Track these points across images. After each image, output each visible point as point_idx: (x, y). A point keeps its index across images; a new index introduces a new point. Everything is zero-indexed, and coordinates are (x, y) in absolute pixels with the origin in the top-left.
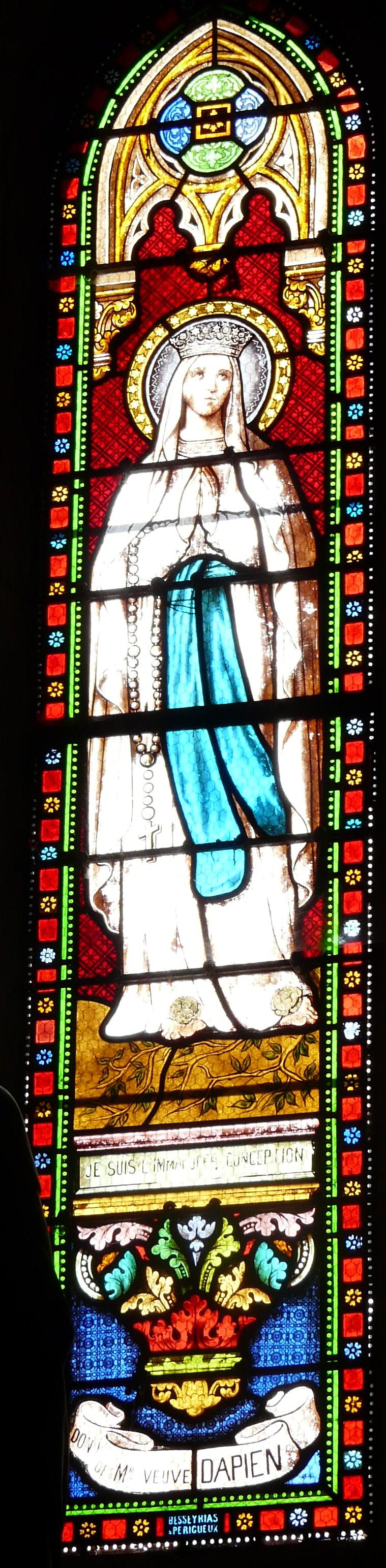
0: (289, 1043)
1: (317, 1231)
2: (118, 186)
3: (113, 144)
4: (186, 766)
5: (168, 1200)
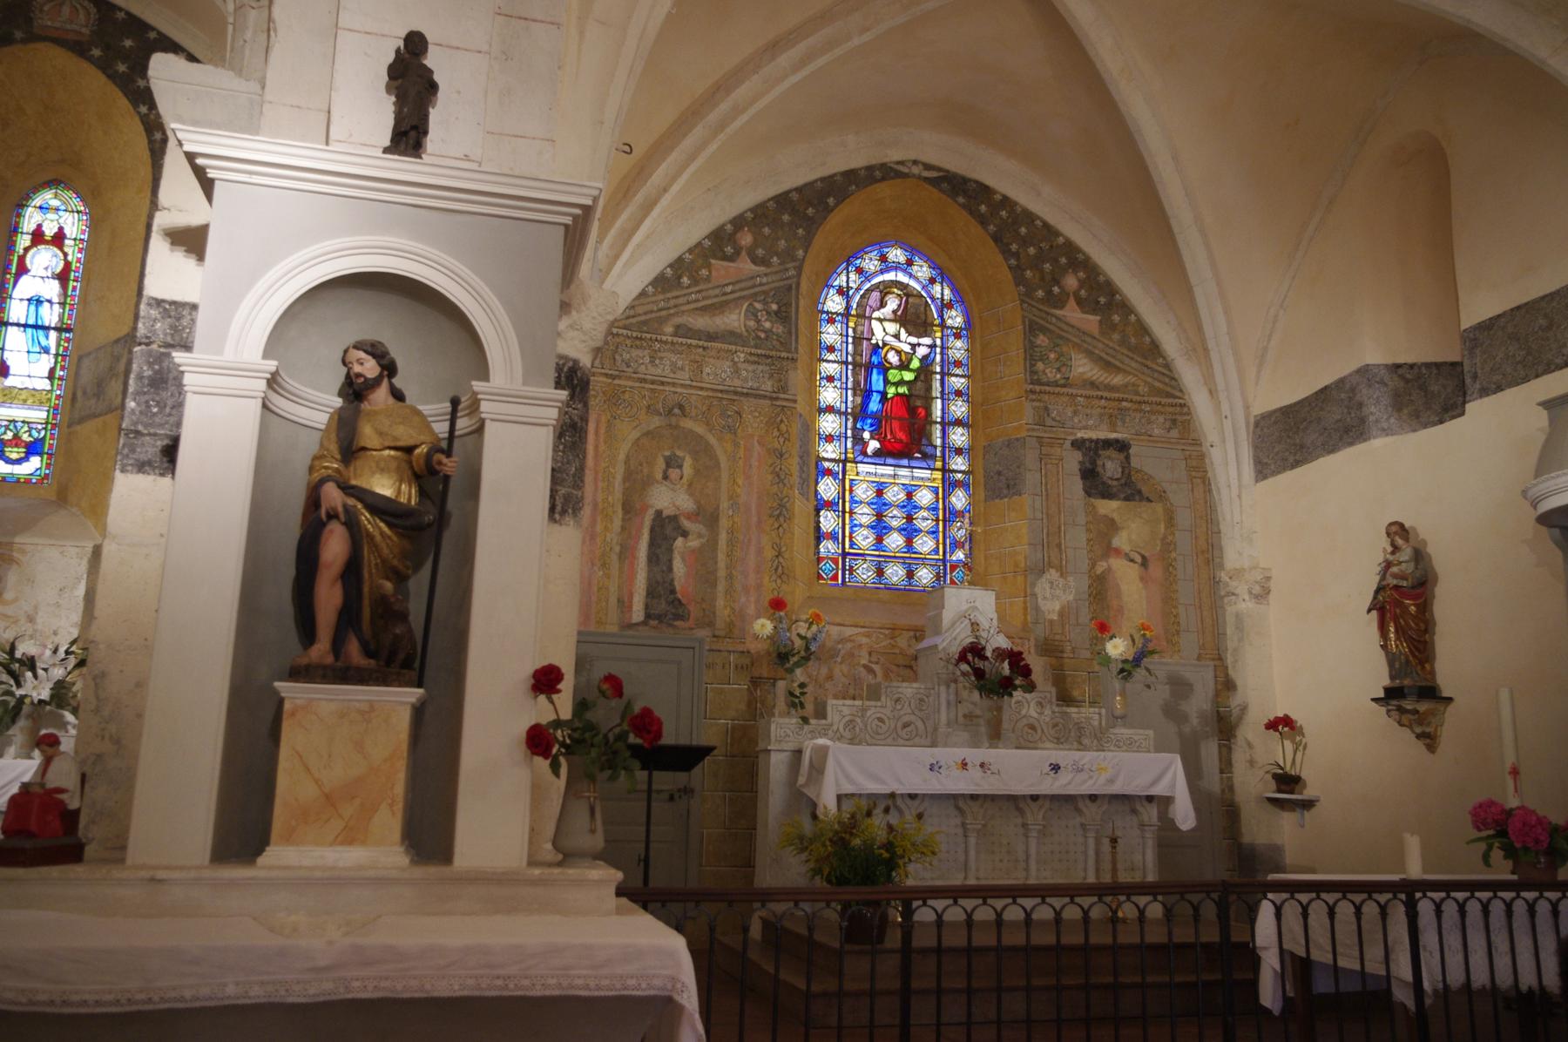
1: (45, 429)
2: (30, 217)
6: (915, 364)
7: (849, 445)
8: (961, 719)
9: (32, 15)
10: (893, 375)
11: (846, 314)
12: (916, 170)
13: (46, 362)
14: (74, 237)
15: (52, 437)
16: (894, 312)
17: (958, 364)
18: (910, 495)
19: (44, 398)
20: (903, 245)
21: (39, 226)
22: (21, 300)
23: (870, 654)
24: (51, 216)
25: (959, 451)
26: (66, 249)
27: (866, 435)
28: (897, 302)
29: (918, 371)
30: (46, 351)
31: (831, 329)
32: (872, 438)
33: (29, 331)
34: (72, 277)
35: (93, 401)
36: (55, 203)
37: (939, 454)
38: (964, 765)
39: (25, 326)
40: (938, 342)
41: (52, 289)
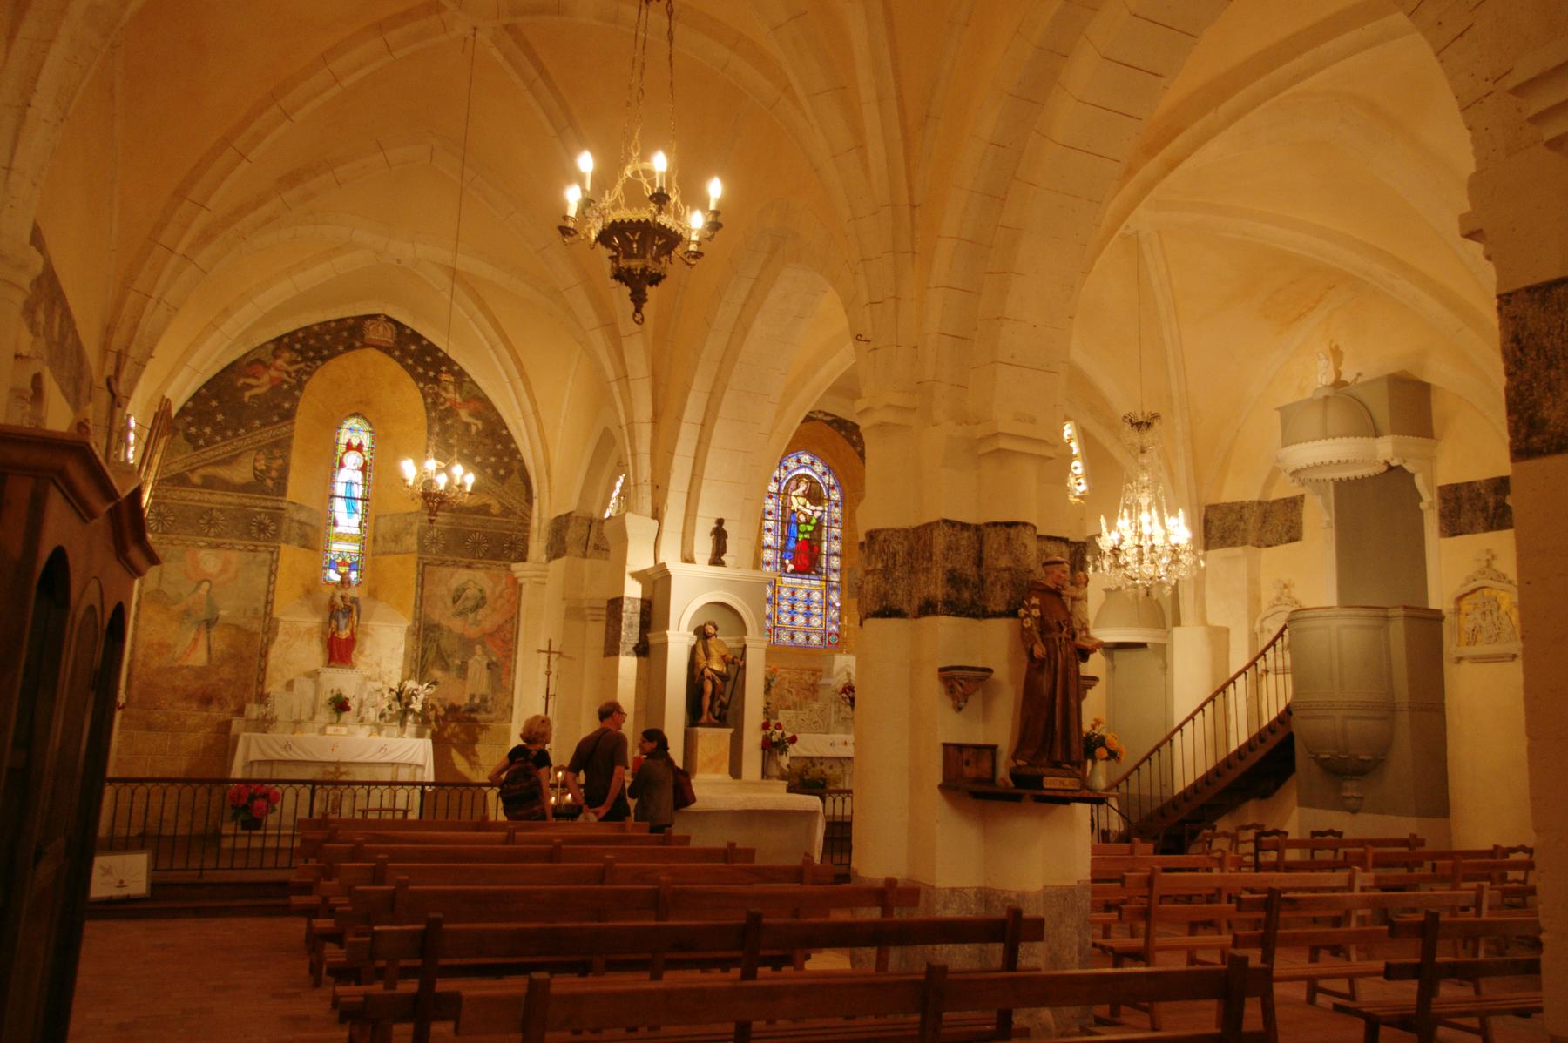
6: (814, 521)
7: (778, 567)
8: (840, 720)
10: (802, 528)
11: (778, 493)
12: (820, 416)
13: (357, 518)
15: (362, 561)
16: (804, 492)
17: (836, 521)
18: (809, 595)
20: (808, 452)
23: (790, 683)
24: (355, 434)
25: (835, 570)
26: (364, 453)
27: (787, 561)
28: (805, 486)
29: (815, 525)
30: (356, 512)
31: (770, 501)
32: (791, 563)
33: (347, 500)
36: (357, 426)
37: (824, 571)
38: (846, 743)
40: (826, 509)
41: (358, 476)
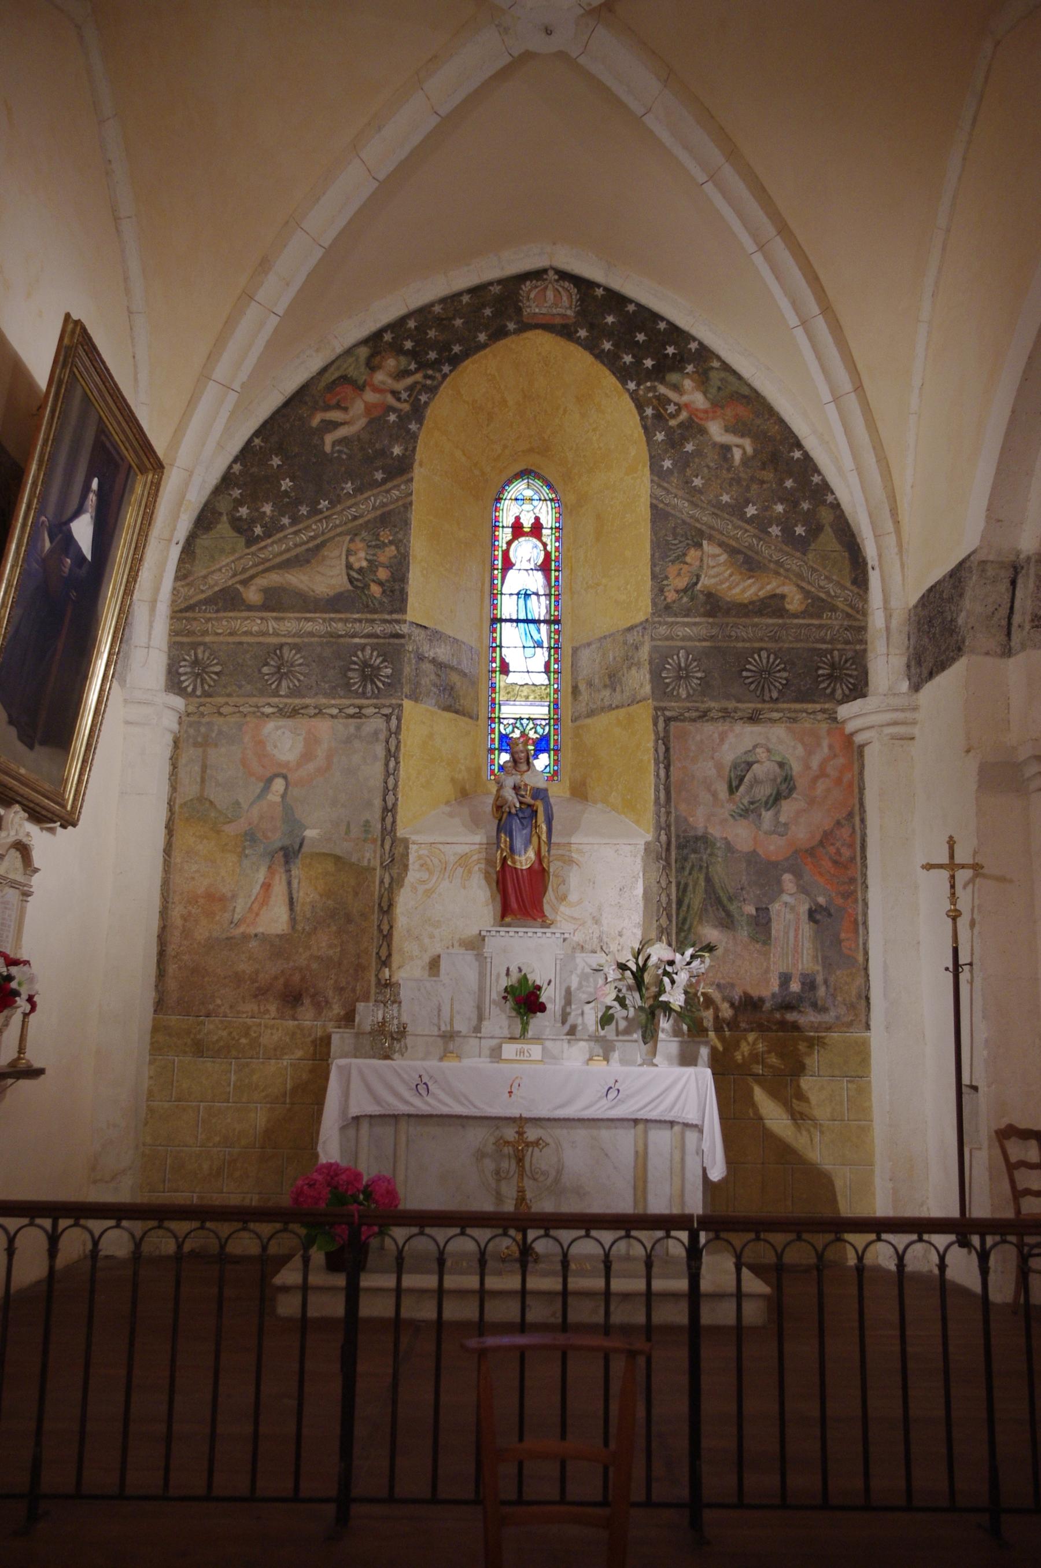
0: (543, 687)
1: (549, 724)
2: (508, 510)
3: (507, 501)
4: (522, 631)
5: (427, 960)
9: (520, 304)
13: (541, 656)
14: (549, 526)
19: (544, 693)
21: (518, 518)
22: (511, 594)
24: (527, 507)
30: (539, 645)
33: (521, 625)
34: (553, 568)
35: (606, 693)
36: (528, 493)
39: (518, 621)
41: (537, 582)
